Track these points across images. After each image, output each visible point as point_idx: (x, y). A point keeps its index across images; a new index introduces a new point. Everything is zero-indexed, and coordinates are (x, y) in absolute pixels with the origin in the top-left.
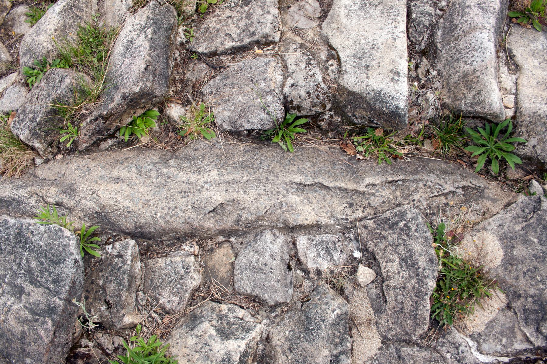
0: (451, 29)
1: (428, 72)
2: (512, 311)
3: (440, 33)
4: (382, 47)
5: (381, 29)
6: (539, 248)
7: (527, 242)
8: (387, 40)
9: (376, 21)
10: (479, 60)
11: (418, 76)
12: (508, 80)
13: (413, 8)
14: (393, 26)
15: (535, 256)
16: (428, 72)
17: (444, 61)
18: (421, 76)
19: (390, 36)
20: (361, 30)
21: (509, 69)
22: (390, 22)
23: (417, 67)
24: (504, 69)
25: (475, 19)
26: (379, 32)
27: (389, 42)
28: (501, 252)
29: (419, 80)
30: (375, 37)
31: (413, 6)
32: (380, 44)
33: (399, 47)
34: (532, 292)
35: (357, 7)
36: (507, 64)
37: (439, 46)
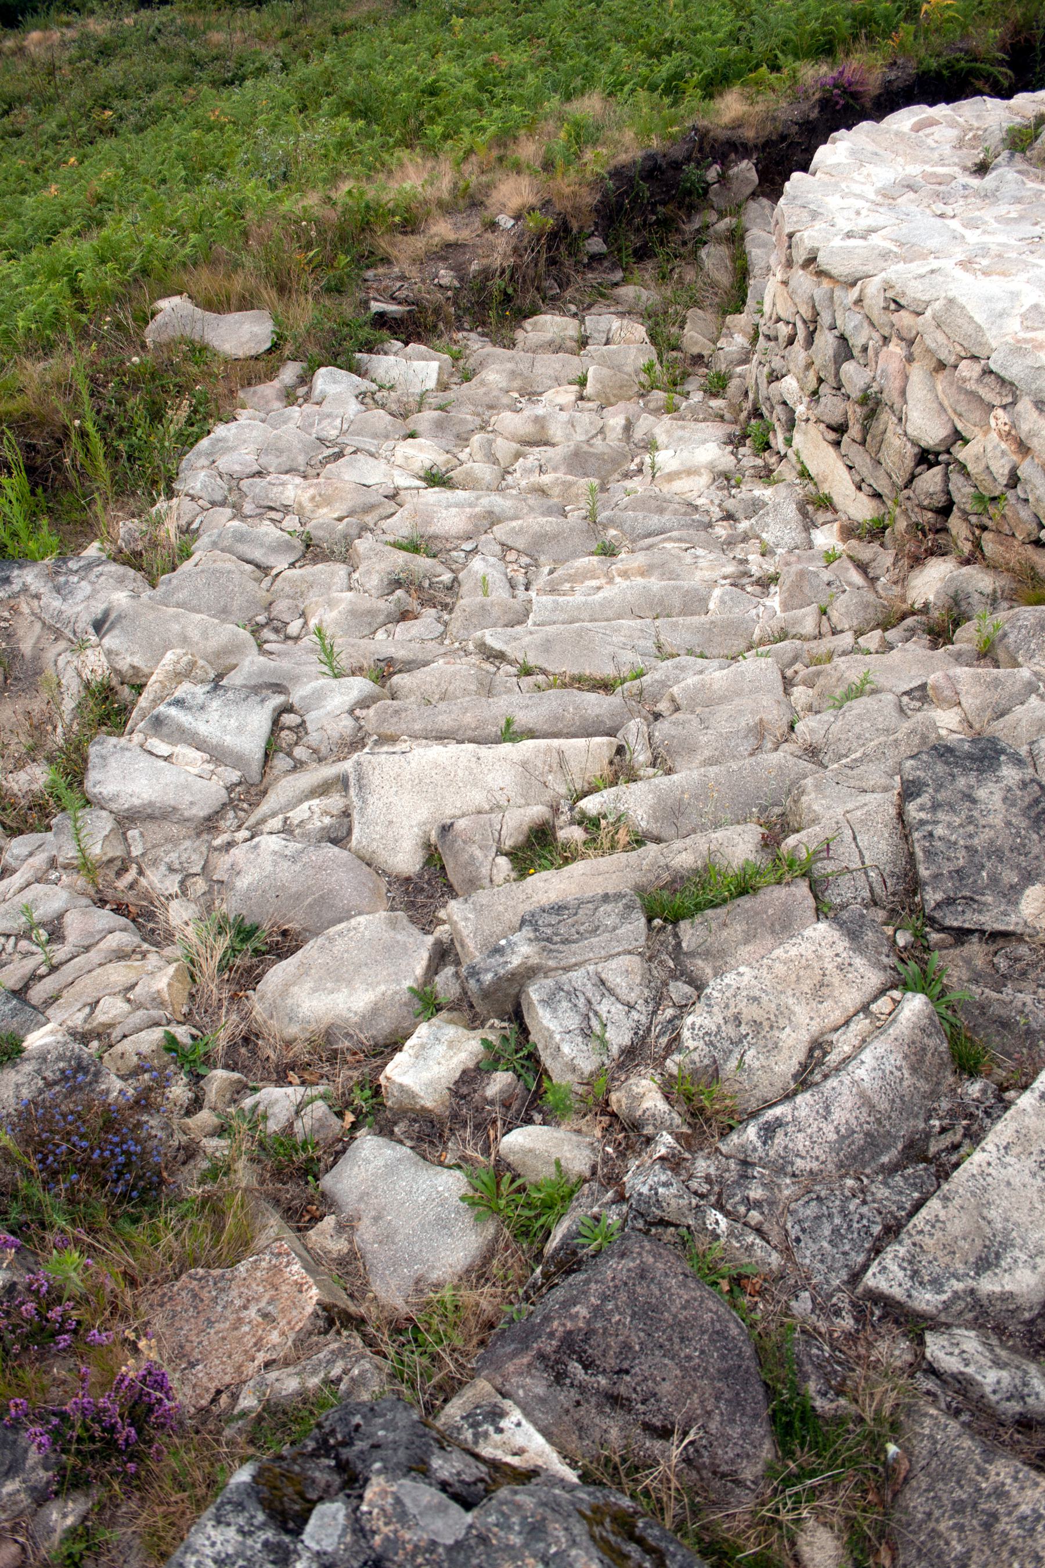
0: (874, 1143)
1: (943, 1130)
2: (834, 1037)
3: (885, 1159)
4: (1035, 1149)
5: (1009, 1183)
6: (988, 865)
7: (994, 880)
8: (1018, 1157)
9: (1005, 1203)
10: (892, 1058)
11: (965, 1136)
12: (844, 1044)
13: (908, 1206)
14: (991, 1170)
15: (1001, 861)
16: (943, 1130)
17: (912, 1122)
18: (960, 1131)
19: (1007, 1159)
20: (1037, 1213)
21: (825, 1054)
22: (989, 1179)
23: (955, 1147)
24: (833, 1058)
25: (849, 1105)
26: (1016, 1182)
27: (1019, 1149)
28: (1027, 892)
29: (967, 1128)
30: (1028, 1179)
31: (904, 1209)
32: (1034, 1157)
33: (1013, 1126)
34: (1035, 837)
35: (1017, 1253)
36: (820, 1063)
37: (900, 1146)
